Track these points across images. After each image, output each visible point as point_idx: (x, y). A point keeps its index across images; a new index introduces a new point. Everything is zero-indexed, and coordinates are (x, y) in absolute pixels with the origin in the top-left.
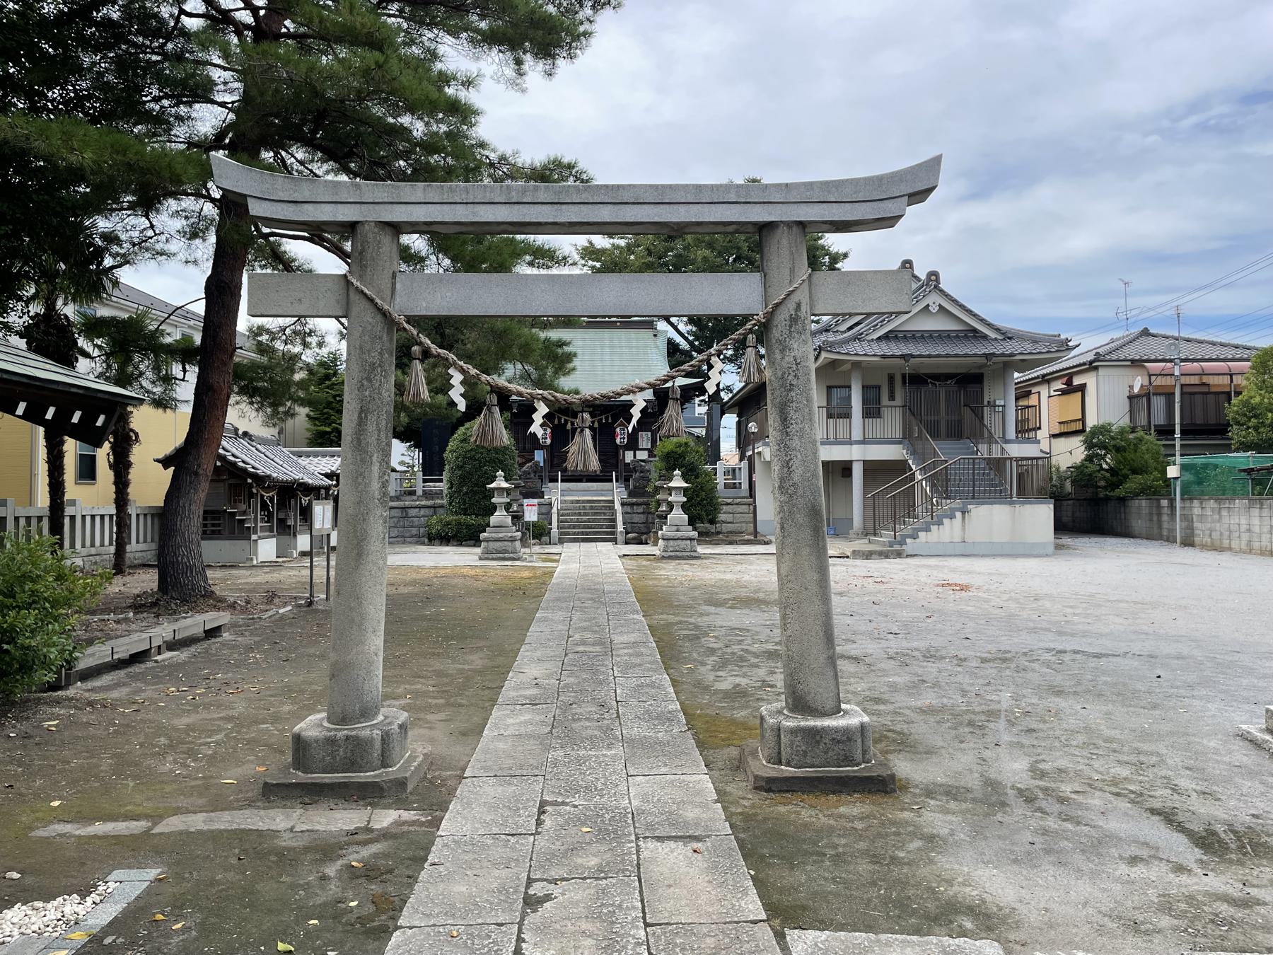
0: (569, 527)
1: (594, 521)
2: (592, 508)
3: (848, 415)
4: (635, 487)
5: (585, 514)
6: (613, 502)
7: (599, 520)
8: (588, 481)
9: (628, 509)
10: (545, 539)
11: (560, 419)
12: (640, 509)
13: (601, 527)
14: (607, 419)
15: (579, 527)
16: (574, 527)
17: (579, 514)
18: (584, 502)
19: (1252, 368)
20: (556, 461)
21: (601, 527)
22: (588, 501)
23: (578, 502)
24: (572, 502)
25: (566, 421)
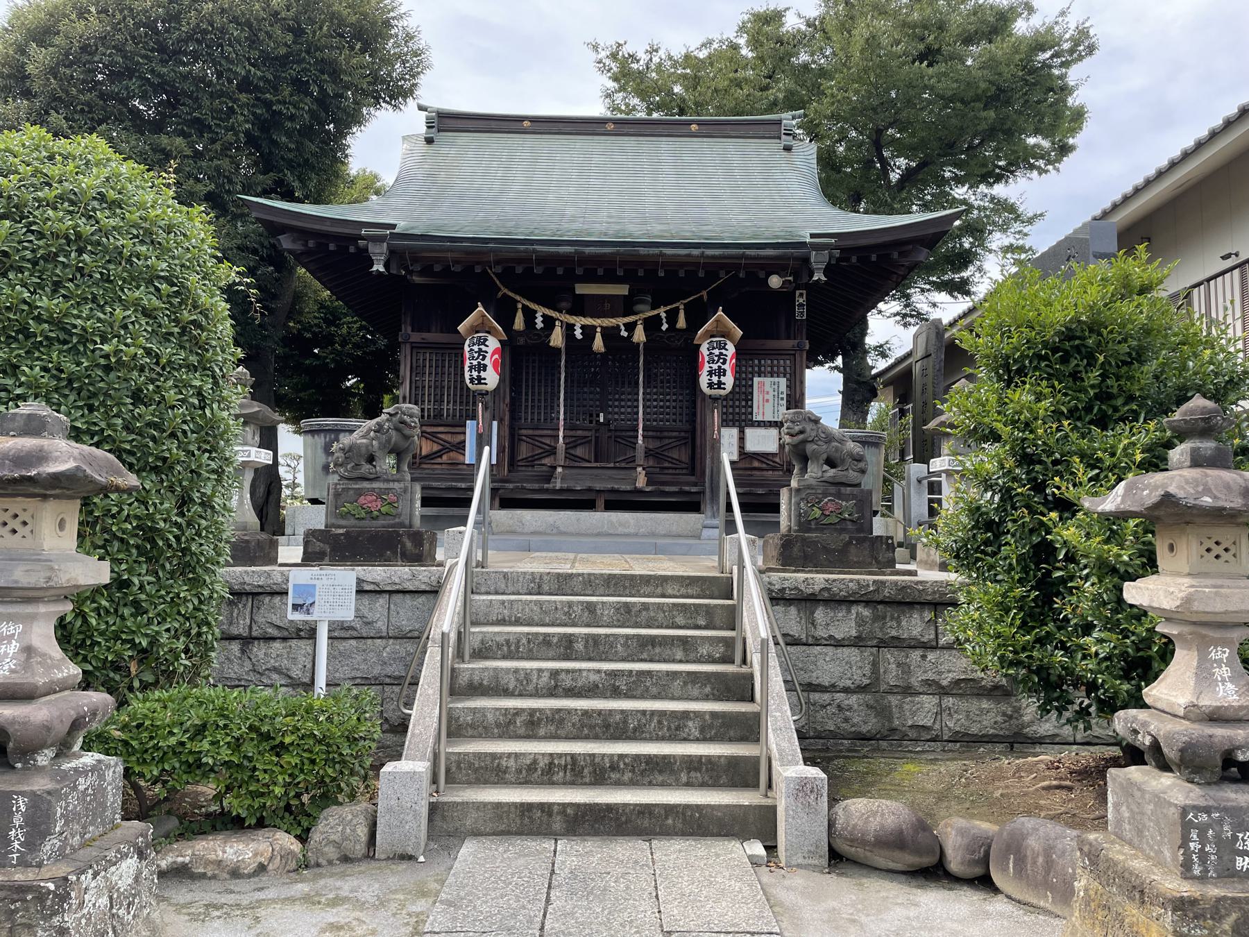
0: (506, 727)
1: (637, 686)
2: (626, 615)
3: (736, 531)
4: (804, 524)
5: (597, 648)
6: (723, 587)
7: (662, 687)
8: (611, 506)
9: (793, 621)
10: (339, 824)
11: (530, 316)
12: (845, 625)
13: (674, 727)
14: (672, 316)
15: (557, 726)
16: (533, 726)
17: (567, 649)
18: (591, 583)
19: (761, 537)
20: (524, 451)
21: (674, 727)
22: (614, 583)
23: (563, 583)
24: (537, 585)
25: (549, 323)
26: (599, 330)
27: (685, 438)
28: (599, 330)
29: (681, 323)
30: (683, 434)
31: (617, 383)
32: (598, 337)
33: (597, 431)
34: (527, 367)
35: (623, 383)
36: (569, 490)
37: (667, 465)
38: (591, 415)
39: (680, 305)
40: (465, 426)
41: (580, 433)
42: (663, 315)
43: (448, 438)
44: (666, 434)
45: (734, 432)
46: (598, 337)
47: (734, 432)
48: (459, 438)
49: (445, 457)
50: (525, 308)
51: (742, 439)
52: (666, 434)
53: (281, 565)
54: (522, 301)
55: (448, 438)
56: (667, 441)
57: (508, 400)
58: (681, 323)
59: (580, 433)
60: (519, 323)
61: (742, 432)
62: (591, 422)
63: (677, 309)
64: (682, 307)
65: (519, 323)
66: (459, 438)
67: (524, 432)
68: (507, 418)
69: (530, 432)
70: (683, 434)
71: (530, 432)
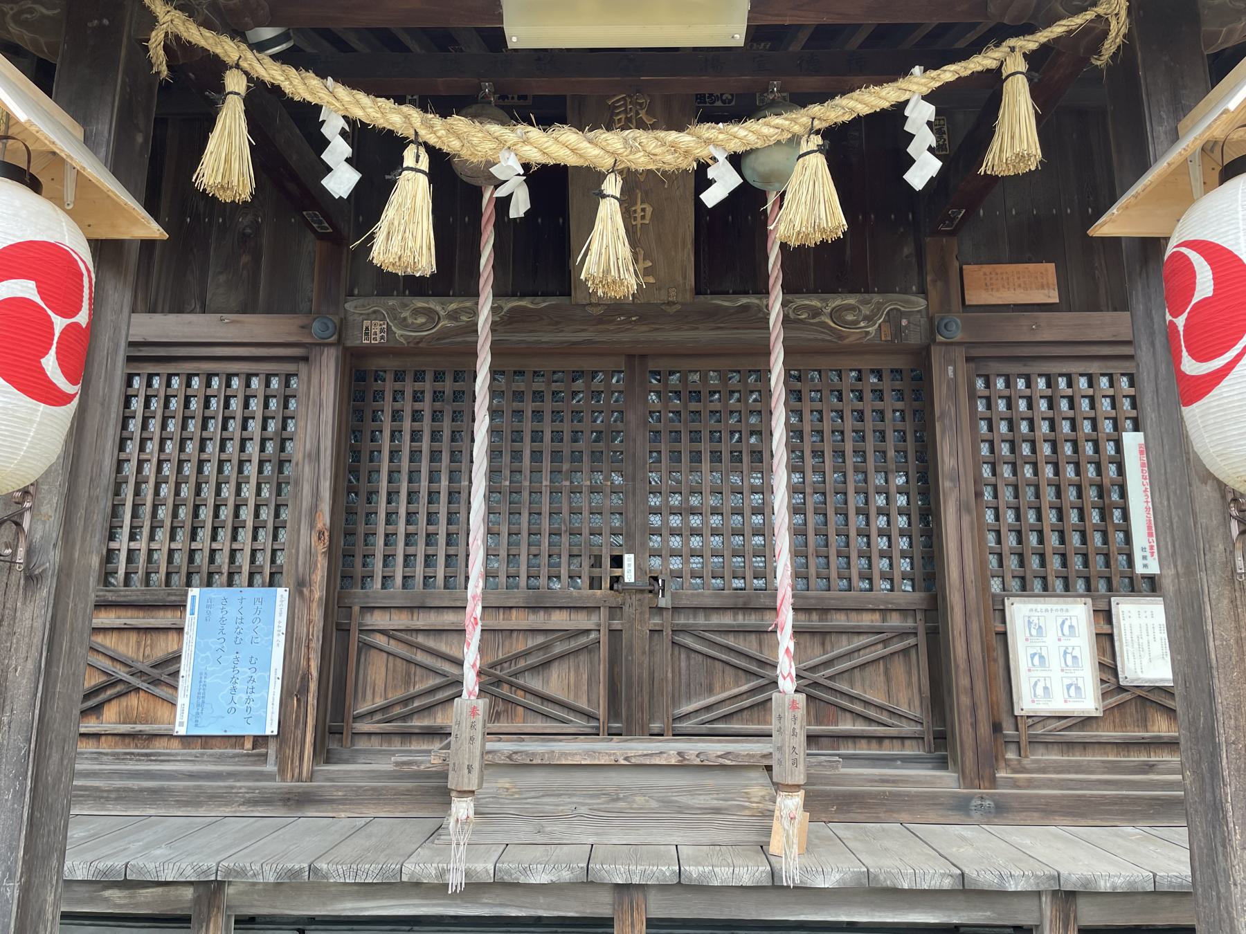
25: (378, 154)
26: (612, 186)
27: (903, 634)
28: (612, 186)
29: (1017, 140)
30: (895, 621)
31: (676, 456)
32: (609, 216)
33: (615, 611)
34: (397, 416)
35: (696, 457)
36: (503, 886)
37: (847, 726)
38: (597, 562)
39: (1011, 58)
40: (181, 606)
41: (559, 620)
42: (920, 115)
43: (126, 647)
44: (840, 620)
45: (1079, 612)
46: (609, 216)
47: (1079, 612)
48: (163, 647)
49: (111, 713)
50: (265, 104)
51: (1106, 640)
52: (840, 620)
53: (961, 270)
54: (247, 64)
55: (126, 647)
56: (844, 645)
57: (324, 519)
58: (1017, 140)
59: (559, 620)
60: (226, 162)
61: (1105, 615)
62: (595, 583)
63: (993, 80)
64: (1017, 64)
65: (226, 162)
66: (163, 647)
67: (379, 620)
68: (319, 576)
69: (399, 621)
70: (895, 621)
71: (399, 621)
